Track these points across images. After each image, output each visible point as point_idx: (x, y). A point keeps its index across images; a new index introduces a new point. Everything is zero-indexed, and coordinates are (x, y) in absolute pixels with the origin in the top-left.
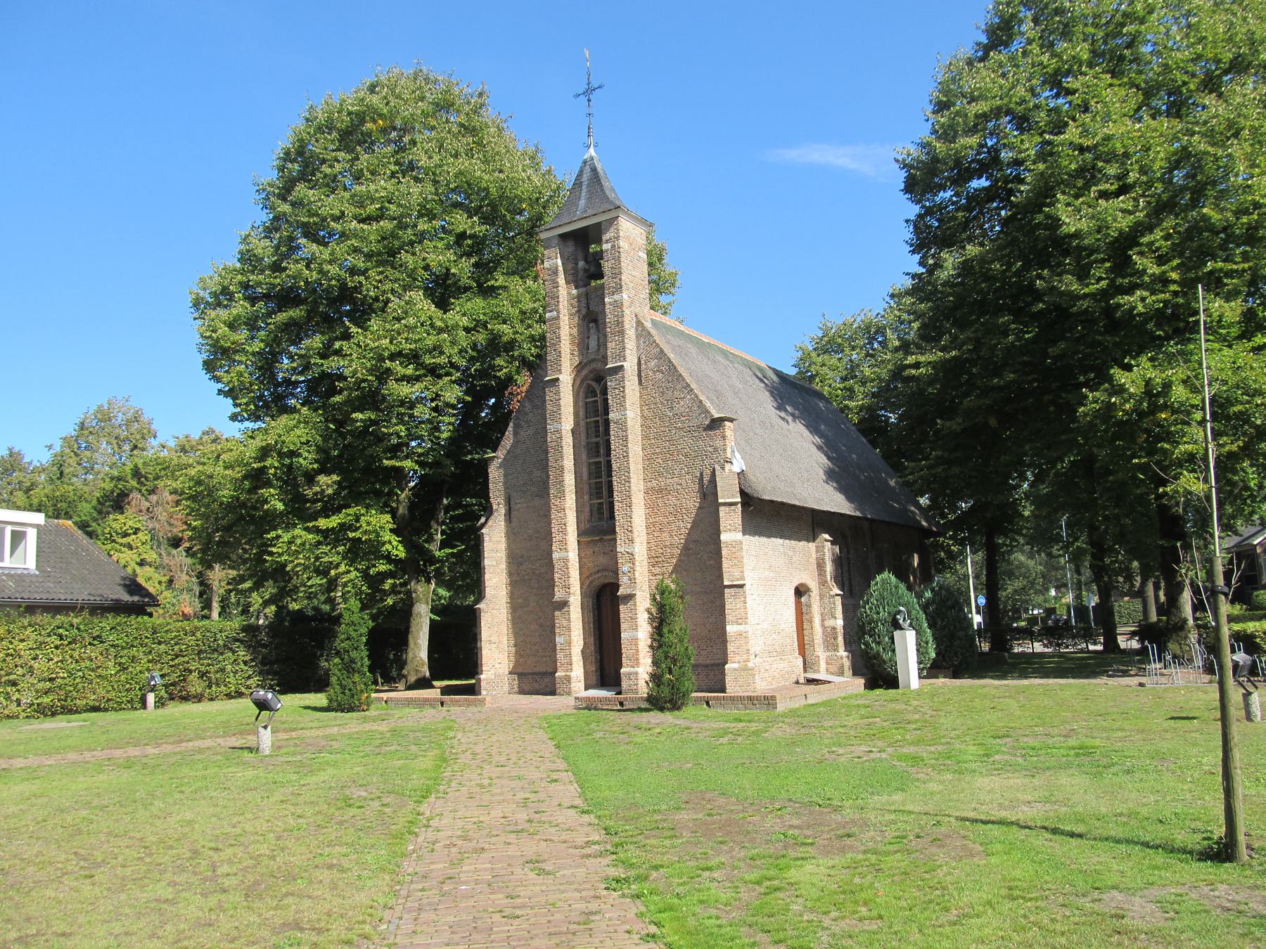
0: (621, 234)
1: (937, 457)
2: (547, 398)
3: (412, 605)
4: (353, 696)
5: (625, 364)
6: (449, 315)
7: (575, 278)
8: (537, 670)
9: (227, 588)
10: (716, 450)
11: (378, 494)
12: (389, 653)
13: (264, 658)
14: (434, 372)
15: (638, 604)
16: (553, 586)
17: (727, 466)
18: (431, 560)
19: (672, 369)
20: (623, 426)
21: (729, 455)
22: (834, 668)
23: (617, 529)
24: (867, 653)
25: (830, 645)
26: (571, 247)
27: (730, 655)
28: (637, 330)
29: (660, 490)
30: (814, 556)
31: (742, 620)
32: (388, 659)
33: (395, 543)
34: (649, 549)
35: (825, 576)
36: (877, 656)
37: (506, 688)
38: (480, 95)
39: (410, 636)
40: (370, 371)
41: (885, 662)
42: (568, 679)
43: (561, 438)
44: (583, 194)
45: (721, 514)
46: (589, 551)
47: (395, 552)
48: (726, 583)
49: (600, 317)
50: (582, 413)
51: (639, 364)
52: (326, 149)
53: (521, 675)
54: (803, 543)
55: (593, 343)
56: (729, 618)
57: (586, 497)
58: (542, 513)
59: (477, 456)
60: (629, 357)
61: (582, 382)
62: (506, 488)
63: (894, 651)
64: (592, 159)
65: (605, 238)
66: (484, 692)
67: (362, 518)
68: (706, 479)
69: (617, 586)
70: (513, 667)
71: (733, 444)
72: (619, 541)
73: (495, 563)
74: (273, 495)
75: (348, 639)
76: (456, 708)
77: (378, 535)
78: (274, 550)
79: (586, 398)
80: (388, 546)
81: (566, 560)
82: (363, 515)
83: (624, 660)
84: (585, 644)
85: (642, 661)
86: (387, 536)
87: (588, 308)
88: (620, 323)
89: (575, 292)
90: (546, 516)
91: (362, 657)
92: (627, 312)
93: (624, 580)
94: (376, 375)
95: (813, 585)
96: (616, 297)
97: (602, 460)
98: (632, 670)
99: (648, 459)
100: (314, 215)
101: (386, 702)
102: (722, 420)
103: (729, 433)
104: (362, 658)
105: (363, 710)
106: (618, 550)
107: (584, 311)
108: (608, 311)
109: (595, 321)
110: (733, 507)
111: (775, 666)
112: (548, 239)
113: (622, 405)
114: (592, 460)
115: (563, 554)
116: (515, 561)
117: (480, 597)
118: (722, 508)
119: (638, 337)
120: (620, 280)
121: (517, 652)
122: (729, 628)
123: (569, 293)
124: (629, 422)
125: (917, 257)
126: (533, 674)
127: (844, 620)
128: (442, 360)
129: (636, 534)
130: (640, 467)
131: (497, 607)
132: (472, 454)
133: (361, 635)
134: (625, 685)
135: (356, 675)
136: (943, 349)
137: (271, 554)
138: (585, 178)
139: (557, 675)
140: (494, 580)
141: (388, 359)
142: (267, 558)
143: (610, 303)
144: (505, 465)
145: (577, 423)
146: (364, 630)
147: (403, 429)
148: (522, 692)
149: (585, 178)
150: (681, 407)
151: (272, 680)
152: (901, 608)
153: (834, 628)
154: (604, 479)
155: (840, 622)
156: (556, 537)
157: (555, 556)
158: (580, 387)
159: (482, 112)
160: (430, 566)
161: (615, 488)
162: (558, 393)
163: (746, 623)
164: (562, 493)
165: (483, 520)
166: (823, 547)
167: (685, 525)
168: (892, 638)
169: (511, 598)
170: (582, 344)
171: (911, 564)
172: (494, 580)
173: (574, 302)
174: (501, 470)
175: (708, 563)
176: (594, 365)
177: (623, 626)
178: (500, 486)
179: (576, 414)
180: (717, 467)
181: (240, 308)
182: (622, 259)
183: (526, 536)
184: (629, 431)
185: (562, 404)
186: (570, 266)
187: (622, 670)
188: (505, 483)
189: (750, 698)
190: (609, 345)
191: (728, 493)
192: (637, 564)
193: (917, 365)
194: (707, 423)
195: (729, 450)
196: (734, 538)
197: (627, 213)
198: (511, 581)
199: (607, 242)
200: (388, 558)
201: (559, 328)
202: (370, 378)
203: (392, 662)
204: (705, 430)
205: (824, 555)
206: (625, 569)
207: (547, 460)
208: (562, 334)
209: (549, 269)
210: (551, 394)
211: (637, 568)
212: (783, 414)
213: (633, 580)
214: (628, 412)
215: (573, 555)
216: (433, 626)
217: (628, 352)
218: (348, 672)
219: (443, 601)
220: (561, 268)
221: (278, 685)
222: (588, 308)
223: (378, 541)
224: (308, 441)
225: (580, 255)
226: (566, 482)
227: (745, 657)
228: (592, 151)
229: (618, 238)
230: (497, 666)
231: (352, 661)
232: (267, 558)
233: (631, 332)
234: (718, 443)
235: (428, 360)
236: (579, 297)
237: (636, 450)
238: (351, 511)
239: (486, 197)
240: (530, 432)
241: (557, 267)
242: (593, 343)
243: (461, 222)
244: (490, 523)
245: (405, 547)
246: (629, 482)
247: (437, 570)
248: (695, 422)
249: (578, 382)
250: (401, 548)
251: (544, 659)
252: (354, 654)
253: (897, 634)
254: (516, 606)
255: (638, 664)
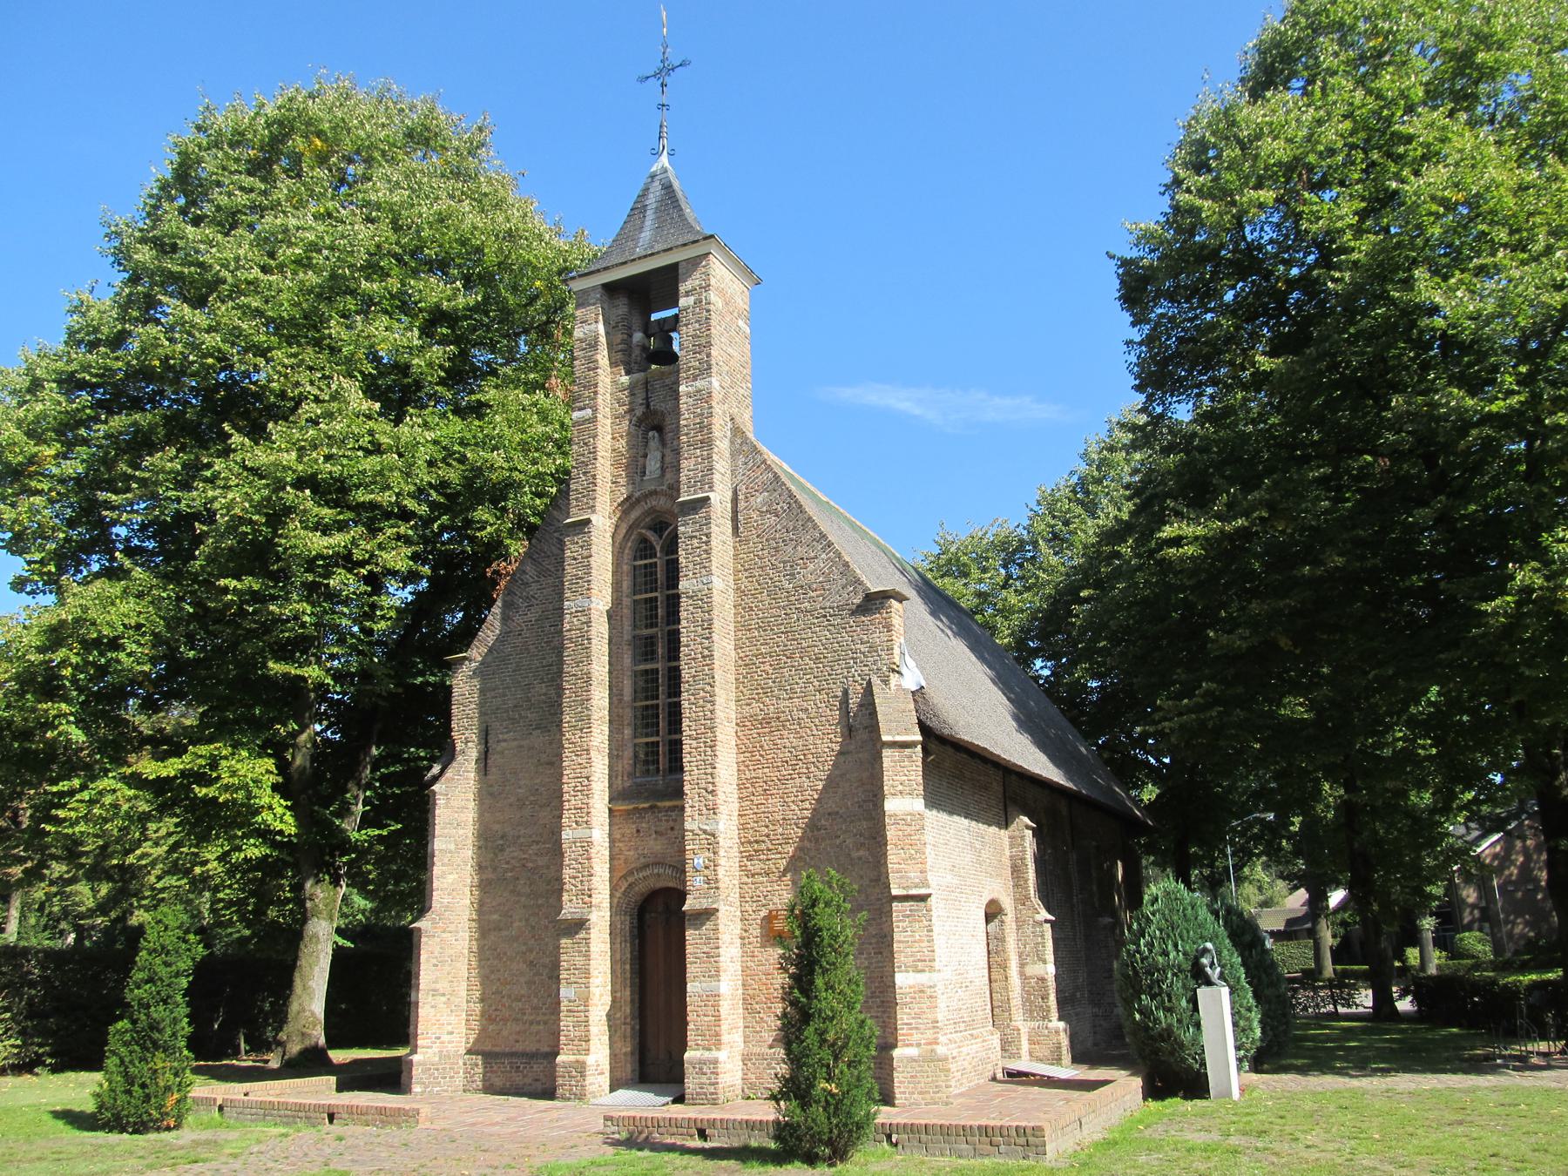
0: (713, 281)
1: (1208, 693)
2: (568, 553)
3: (304, 920)
4: (147, 1098)
5: (711, 495)
6: (404, 429)
7: (625, 357)
8: (519, 1047)
9: (47, 889)
10: (873, 648)
11: (258, 726)
12: (263, 1001)
13: (30, 1003)
14: (373, 517)
15: (721, 927)
16: (560, 892)
17: (894, 678)
18: (344, 845)
19: (795, 507)
20: (704, 602)
21: (897, 660)
22: (1043, 1051)
23: (687, 788)
24: (1147, 1028)
25: (1034, 1010)
26: (622, 307)
27: (902, 1031)
28: (732, 442)
29: (766, 721)
30: (1007, 853)
31: (925, 963)
32: (261, 1010)
33: (279, 810)
34: (743, 827)
35: (1026, 889)
36: (1168, 1034)
37: (459, 1081)
38: (480, 129)
39: (297, 974)
40: (258, 508)
41: (1182, 1046)
42: (581, 1068)
43: (588, 623)
44: (648, 223)
45: (886, 763)
46: (630, 829)
47: (278, 826)
48: (895, 892)
49: (668, 420)
50: (626, 585)
51: (735, 500)
52: (224, 169)
53: (489, 1057)
54: (993, 829)
55: (653, 465)
56: (900, 958)
57: (628, 732)
58: (544, 758)
59: (432, 679)
60: (718, 486)
61: (631, 528)
62: (482, 714)
63: (1198, 1025)
64: (665, 171)
65: (682, 288)
66: (416, 1088)
67: (224, 763)
68: (854, 701)
69: (681, 896)
70: (477, 1041)
71: (902, 641)
72: (688, 811)
73: (452, 847)
74: (65, 715)
75: (150, 980)
76: (360, 1129)
77: (249, 796)
78: (61, 813)
79: (635, 560)
80: (266, 816)
81: (587, 844)
82: (226, 758)
83: (691, 1036)
84: (614, 1001)
85: (725, 1038)
86: (265, 797)
87: (648, 406)
88: (704, 427)
89: (625, 379)
90: (551, 764)
91: (177, 1020)
92: (718, 409)
93: (695, 882)
94: (266, 515)
95: (1007, 903)
96: (699, 384)
97: (659, 666)
98: (707, 1054)
99: (747, 665)
100: (191, 264)
101: (221, 1108)
102: (885, 596)
103: (896, 621)
104: (175, 1021)
105: (168, 1129)
106: (687, 826)
107: (639, 412)
108: (683, 407)
109: (659, 429)
110: (907, 751)
111: (965, 1050)
112: (584, 292)
113: (704, 566)
114: (642, 667)
115: (581, 832)
116: (490, 843)
117: (422, 908)
118: (886, 753)
119: (734, 454)
120: (709, 355)
121: (483, 1013)
122: (900, 979)
123: (614, 382)
124: (717, 598)
125: (1142, 398)
126: (513, 1055)
127: (1058, 962)
128: (386, 498)
129: (721, 797)
130: (732, 678)
131: (452, 927)
132: (423, 675)
133: (177, 975)
134: (691, 1084)
135: (160, 1055)
136: (1219, 517)
137: (57, 821)
138: (652, 200)
139: (559, 1059)
140: (450, 878)
141: (293, 486)
142: (48, 828)
143: (689, 395)
144: (482, 672)
145: (617, 602)
146: (185, 964)
147: (309, 609)
148: (489, 1089)
149: (652, 200)
150: (809, 573)
151: (40, 1045)
152: (1209, 945)
153: (1043, 980)
154: (662, 700)
155: (1051, 969)
156: (571, 801)
157: (567, 835)
158: (626, 537)
159: (482, 152)
160: (341, 855)
161: (686, 713)
162: (588, 545)
163: (932, 969)
164: (585, 722)
165: (436, 769)
166: (1023, 838)
167: (810, 784)
168: (1194, 1001)
169: (480, 912)
170: (635, 467)
171: (1115, 876)
172: (450, 878)
173: (624, 396)
174: (476, 682)
175: (855, 854)
176: (652, 502)
177: (692, 969)
178: (472, 709)
179: (616, 586)
180: (875, 680)
181: (51, 402)
182: (713, 323)
183: (512, 799)
184: (715, 612)
185: (593, 564)
186: (619, 337)
187: (687, 1055)
188: (481, 705)
189: (985, 1131)
190: (684, 464)
191: (898, 724)
192: (722, 853)
193: (1177, 542)
194: (857, 601)
195: (896, 651)
196: (909, 809)
197: (725, 249)
198: (481, 881)
199: (687, 294)
200: (265, 834)
201: (595, 437)
202: (255, 518)
203: (266, 1015)
204: (853, 613)
205: (1024, 851)
206: (699, 861)
207: (561, 662)
208: (600, 447)
209: (581, 341)
210: (574, 548)
211: (722, 861)
212: (939, 623)
213: (712, 883)
214: (714, 579)
215: (599, 833)
216: (339, 954)
217: (717, 477)
218: (144, 1048)
219: (360, 917)
220: (603, 339)
221: (51, 1055)
222: (648, 406)
223: (249, 806)
224: (138, 627)
225: (636, 321)
226: (594, 702)
227: (929, 1034)
228: (664, 160)
229: (707, 287)
230: (446, 1038)
231: (154, 1026)
232: (48, 828)
233: (722, 445)
234: (878, 637)
235: (361, 496)
236: (632, 388)
237: (724, 646)
238: (203, 750)
239: (479, 262)
240: (532, 616)
241: (596, 338)
242: (653, 465)
243: (434, 291)
244: (449, 773)
245: (296, 817)
246: (713, 703)
247: (350, 864)
248: (836, 600)
249: (623, 531)
250: (289, 818)
251: (535, 1028)
252: (158, 1012)
253: (1203, 993)
254: (488, 927)
255: (718, 1044)
